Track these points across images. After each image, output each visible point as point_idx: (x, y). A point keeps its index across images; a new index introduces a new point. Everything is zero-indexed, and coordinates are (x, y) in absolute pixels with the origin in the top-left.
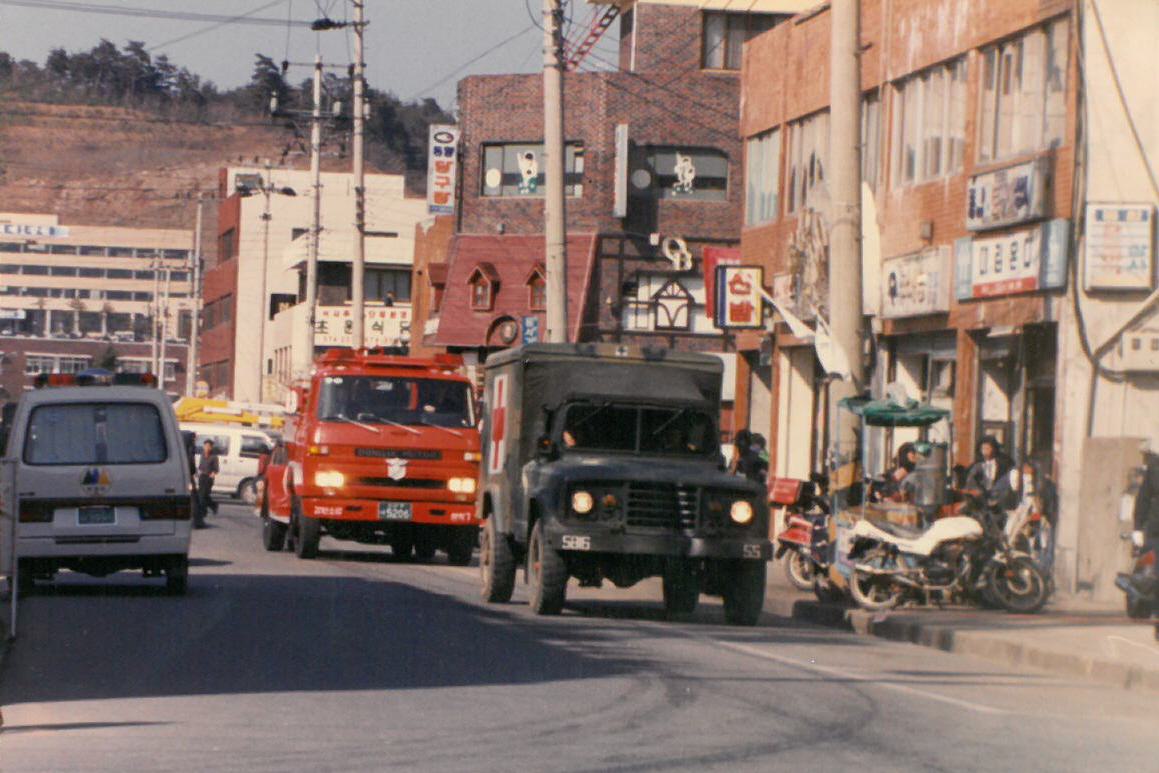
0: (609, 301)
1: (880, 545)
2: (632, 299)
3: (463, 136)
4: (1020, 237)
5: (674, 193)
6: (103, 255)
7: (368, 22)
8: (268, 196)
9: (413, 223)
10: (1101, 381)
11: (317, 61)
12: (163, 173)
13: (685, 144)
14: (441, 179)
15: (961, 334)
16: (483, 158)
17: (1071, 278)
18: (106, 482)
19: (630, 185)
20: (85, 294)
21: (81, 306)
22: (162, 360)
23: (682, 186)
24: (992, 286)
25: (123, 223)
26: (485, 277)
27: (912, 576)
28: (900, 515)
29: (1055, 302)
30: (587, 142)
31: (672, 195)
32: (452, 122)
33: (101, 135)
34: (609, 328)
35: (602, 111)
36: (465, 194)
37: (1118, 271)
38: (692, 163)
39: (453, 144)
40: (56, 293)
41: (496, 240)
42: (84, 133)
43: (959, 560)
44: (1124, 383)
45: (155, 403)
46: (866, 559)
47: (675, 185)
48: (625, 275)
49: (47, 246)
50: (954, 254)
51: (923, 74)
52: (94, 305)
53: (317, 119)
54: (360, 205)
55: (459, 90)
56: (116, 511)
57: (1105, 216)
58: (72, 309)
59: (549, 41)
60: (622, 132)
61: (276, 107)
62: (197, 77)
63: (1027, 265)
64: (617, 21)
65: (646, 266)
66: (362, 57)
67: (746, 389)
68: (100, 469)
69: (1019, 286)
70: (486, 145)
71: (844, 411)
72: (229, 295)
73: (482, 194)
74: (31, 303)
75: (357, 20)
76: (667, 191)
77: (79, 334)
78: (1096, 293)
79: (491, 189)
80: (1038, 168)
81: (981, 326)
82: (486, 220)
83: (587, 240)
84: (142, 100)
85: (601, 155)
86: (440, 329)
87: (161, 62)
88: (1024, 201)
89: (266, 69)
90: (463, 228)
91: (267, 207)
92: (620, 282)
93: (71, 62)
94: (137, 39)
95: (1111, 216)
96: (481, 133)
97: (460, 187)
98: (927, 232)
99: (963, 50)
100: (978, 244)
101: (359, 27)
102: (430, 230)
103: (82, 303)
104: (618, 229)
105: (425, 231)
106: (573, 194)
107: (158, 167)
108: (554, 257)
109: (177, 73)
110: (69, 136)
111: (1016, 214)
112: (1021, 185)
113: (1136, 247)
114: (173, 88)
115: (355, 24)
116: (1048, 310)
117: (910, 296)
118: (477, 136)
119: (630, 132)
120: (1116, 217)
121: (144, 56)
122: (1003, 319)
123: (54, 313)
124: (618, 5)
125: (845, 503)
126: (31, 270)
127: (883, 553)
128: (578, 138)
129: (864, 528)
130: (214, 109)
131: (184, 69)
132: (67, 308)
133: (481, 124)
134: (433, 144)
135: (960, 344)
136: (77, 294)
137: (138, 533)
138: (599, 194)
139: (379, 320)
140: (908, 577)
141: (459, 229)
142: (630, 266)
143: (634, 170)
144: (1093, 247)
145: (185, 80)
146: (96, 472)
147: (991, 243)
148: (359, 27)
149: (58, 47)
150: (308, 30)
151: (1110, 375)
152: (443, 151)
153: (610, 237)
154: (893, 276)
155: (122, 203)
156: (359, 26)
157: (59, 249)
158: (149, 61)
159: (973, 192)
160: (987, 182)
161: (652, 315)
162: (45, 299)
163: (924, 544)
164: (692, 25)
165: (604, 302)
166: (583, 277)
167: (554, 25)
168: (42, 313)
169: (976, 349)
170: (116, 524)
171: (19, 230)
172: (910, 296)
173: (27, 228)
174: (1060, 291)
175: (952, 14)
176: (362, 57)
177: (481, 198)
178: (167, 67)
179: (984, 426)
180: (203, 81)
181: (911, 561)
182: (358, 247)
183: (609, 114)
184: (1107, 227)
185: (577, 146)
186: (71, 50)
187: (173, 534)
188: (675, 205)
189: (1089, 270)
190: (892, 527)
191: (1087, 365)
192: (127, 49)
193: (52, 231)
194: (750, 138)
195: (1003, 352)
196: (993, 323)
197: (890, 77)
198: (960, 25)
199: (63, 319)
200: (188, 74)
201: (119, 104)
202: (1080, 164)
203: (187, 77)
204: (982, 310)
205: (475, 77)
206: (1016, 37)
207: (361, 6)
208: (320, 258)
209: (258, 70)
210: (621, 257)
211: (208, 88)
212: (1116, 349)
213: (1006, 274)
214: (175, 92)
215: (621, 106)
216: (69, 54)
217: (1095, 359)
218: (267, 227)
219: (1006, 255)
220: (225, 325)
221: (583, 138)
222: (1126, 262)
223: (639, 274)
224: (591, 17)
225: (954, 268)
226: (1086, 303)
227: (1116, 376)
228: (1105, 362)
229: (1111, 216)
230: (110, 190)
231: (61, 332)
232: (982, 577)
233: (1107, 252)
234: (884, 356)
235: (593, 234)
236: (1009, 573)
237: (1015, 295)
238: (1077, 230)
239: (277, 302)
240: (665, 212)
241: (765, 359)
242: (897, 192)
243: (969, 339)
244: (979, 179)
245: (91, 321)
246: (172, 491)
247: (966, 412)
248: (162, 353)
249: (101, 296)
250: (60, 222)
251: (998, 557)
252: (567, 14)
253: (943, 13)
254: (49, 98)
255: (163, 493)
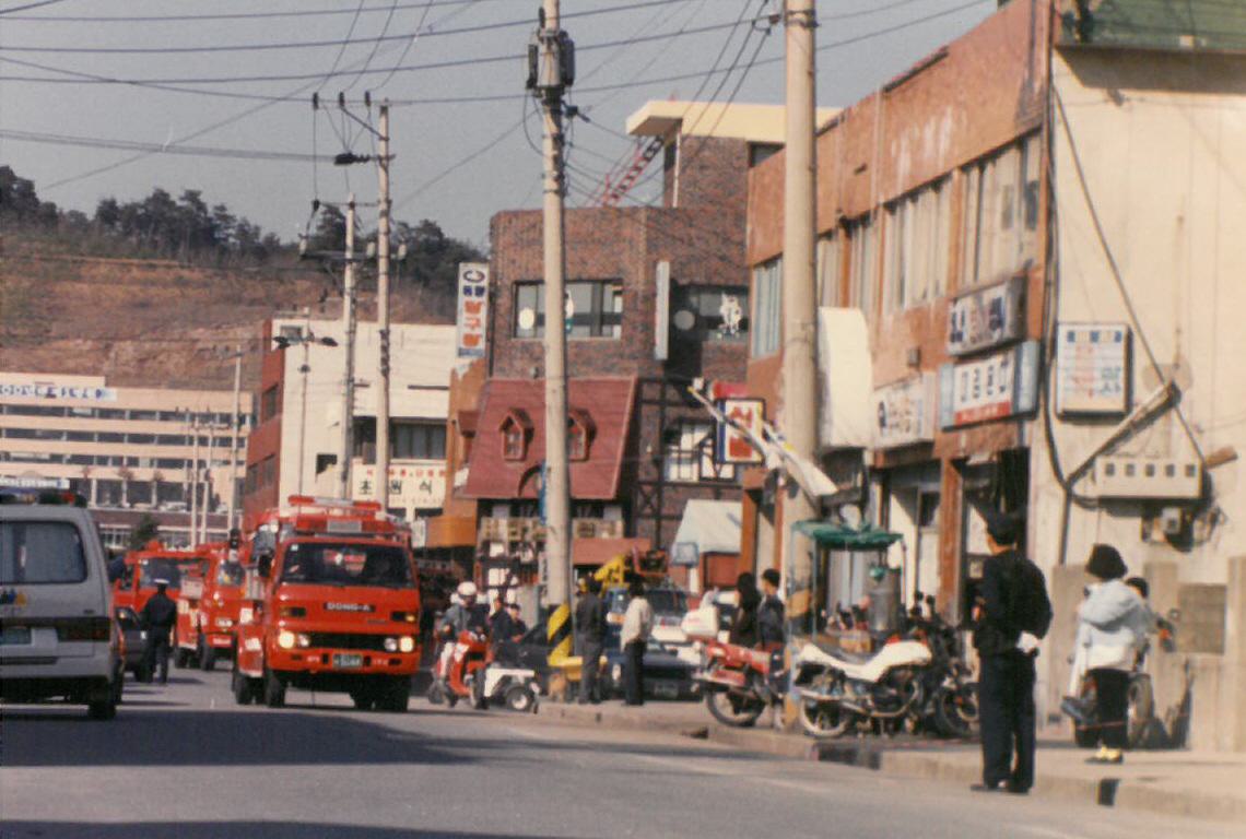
0: (649, 449)
1: (826, 671)
2: (674, 448)
3: (494, 274)
4: (996, 360)
5: (720, 336)
6: (154, 420)
7: (393, 157)
8: (306, 346)
9: (449, 370)
10: (1075, 509)
11: (349, 200)
12: (220, 331)
13: (731, 283)
14: (472, 319)
15: (945, 465)
16: (515, 298)
17: (1042, 402)
18: (23, 601)
19: (672, 327)
20: (134, 462)
21: (130, 476)
22: (203, 529)
23: (728, 328)
24: (970, 412)
25: (176, 385)
26: (516, 423)
27: (860, 702)
28: (853, 641)
29: (1028, 427)
30: (626, 280)
31: (717, 337)
32: (483, 261)
33: (153, 291)
34: (649, 478)
35: (642, 247)
36: (497, 336)
37: (1091, 393)
38: (739, 305)
39: (485, 283)
40: (103, 461)
41: (527, 384)
42: (135, 288)
43: (909, 688)
44: (1097, 510)
45: (71, 520)
46: (814, 685)
47: (721, 326)
48: (667, 422)
49: (93, 409)
50: (939, 377)
51: (913, 195)
52: (143, 474)
53: (350, 261)
54: (385, 349)
55: (492, 227)
56: (34, 632)
57: (1077, 337)
58: (122, 478)
59: (548, 166)
60: (664, 270)
61: (325, 259)
62: (257, 229)
63: (1002, 389)
64: (660, 159)
65: (690, 413)
66: (387, 193)
67: (751, 530)
68: (18, 589)
69: (994, 412)
70: (519, 283)
71: (798, 535)
72: (272, 456)
73: (515, 336)
74: (76, 471)
75: (382, 154)
76: (712, 333)
77: (127, 505)
78: (1070, 417)
79: (524, 330)
80: (1010, 290)
81: (961, 455)
82: (518, 364)
83: (625, 384)
84: (197, 254)
85: (640, 294)
86: (469, 479)
87: (219, 212)
88: (999, 323)
89: (332, 220)
90: (495, 373)
91: (306, 358)
92: (661, 429)
93: (122, 212)
94: (192, 188)
95: (1083, 333)
96: (513, 271)
97: (492, 327)
98: (914, 359)
99: (947, 170)
100: (960, 370)
101: (384, 162)
102: (465, 376)
103: (627, 645)
104: (659, 373)
105: (460, 377)
106: (612, 334)
107: (214, 325)
108: (554, 391)
109: (236, 224)
110: (119, 293)
111: (991, 337)
112: (996, 306)
113: (1109, 369)
114: (231, 240)
115: (380, 158)
116: (1021, 435)
117: (897, 425)
118: (508, 276)
119: (673, 270)
120: (1088, 338)
121: (201, 207)
122: (981, 448)
123: (100, 482)
124: (662, 137)
125: (799, 630)
126: (75, 436)
127: (830, 679)
128: (617, 276)
129: (811, 653)
130: (277, 262)
131: (244, 220)
132: (115, 477)
133: (513, 262)
134: (462, 283)
135: (944, 478)
136: (125, 462)
137: (54, 654)
138: (641, 336)
139: (427, 479)
140: (856, 703)
141: (491, 374)
142: (672, 412)
143: (676, 311)
144: (1066, 369)
145: (246, 232)
146: (13, 592)
147: (970, 368)
148: (384, 162)
149: (108, 197)
150: (331, 165)
151: (1085, 503)
152: (474, 291)
153: (651, 381)
154: (882, 406)
155: (175, 362)
156: (384, 161)
157: (106, 414)
158: (206, 212)
159: (954, 315)
160: (966, 304)
161: (695, 466)
162: (90, 467)
163: (872, 670)
164: (738, 158)
165: (645, 450)
166: (620, 424)
167: (554, 148)
168: (87, 482)
169: (960, 480)
170: (33, 644)
171: (63, 393)
172: (897, 425)
173: (71, 392)
174: (1031, 415)
175: (937, 133)
176: (387, 193)
177: (513, 340)
178: (226, 218)
179: (969, 559)
180: (263, 234)
181: (860, 688)
182: (383, 392)
183: (649, 251)
184: (1078, 349)
185: (615, 284)
186: (123, 199)
187: (93, 655)
188: (721, 349)
189: (1060, 395)
190: (840, 652)
191: (1060, 492)
192: (182, 199)
193: (99, 393)
194: (757, 266)
195: (984, 483)
196: (973, 452)
197: (882, 200)
198: (944, 144)
199: (110, 489)
200: (248, 225)
201: (174, 257)
202: (1052, 284)
203: (246, 228)
204: (963, 438)
205: (507, 213)
206: (994, 155)
207: (386, 139)
208: (357, 413)
209: (324, 220)
210: (662, 403)
211: (271, 241)
212: (1089, 472)
213: (984, 400)
214: (234, 244)
215: (662, 243)
216: (119, 204)
217: (1068, 486)
218: (305, 380)
219: (984, 380)
220: (268, 488)
221: (621, 276)
222: (1099, 385)
223: (681, 421)
224: (632, 153)
225: (939, 396)
226: (1059, 429)
227: (1091, 504)
228: (1079, 489)
229: (1083, 333)
230: (163, 350)
231: (108, 503)
232: (930, 703)
233: (1079, 374)
234: (876, 490)
235: (632, 378)
236: (958, 700)
237: (991, 421)
238: (1048, 351)
239: (324, 462)
240: (710, 355)
241: (769, 497)
242: (888, 319)
243: (953, 469)
244: (959, 303)
245: (139, 491)
246: (91, 611)
247: (951, 544)
248: (204, 524)
249: (151, 464)
250: (107, 384)
251: (947, 683)
252: (568, 138)
253: (929, 133)
254: (98, 251)
255: (82, 615)
